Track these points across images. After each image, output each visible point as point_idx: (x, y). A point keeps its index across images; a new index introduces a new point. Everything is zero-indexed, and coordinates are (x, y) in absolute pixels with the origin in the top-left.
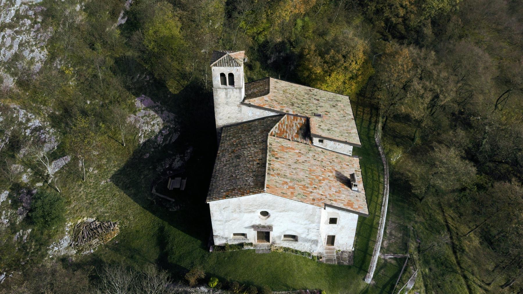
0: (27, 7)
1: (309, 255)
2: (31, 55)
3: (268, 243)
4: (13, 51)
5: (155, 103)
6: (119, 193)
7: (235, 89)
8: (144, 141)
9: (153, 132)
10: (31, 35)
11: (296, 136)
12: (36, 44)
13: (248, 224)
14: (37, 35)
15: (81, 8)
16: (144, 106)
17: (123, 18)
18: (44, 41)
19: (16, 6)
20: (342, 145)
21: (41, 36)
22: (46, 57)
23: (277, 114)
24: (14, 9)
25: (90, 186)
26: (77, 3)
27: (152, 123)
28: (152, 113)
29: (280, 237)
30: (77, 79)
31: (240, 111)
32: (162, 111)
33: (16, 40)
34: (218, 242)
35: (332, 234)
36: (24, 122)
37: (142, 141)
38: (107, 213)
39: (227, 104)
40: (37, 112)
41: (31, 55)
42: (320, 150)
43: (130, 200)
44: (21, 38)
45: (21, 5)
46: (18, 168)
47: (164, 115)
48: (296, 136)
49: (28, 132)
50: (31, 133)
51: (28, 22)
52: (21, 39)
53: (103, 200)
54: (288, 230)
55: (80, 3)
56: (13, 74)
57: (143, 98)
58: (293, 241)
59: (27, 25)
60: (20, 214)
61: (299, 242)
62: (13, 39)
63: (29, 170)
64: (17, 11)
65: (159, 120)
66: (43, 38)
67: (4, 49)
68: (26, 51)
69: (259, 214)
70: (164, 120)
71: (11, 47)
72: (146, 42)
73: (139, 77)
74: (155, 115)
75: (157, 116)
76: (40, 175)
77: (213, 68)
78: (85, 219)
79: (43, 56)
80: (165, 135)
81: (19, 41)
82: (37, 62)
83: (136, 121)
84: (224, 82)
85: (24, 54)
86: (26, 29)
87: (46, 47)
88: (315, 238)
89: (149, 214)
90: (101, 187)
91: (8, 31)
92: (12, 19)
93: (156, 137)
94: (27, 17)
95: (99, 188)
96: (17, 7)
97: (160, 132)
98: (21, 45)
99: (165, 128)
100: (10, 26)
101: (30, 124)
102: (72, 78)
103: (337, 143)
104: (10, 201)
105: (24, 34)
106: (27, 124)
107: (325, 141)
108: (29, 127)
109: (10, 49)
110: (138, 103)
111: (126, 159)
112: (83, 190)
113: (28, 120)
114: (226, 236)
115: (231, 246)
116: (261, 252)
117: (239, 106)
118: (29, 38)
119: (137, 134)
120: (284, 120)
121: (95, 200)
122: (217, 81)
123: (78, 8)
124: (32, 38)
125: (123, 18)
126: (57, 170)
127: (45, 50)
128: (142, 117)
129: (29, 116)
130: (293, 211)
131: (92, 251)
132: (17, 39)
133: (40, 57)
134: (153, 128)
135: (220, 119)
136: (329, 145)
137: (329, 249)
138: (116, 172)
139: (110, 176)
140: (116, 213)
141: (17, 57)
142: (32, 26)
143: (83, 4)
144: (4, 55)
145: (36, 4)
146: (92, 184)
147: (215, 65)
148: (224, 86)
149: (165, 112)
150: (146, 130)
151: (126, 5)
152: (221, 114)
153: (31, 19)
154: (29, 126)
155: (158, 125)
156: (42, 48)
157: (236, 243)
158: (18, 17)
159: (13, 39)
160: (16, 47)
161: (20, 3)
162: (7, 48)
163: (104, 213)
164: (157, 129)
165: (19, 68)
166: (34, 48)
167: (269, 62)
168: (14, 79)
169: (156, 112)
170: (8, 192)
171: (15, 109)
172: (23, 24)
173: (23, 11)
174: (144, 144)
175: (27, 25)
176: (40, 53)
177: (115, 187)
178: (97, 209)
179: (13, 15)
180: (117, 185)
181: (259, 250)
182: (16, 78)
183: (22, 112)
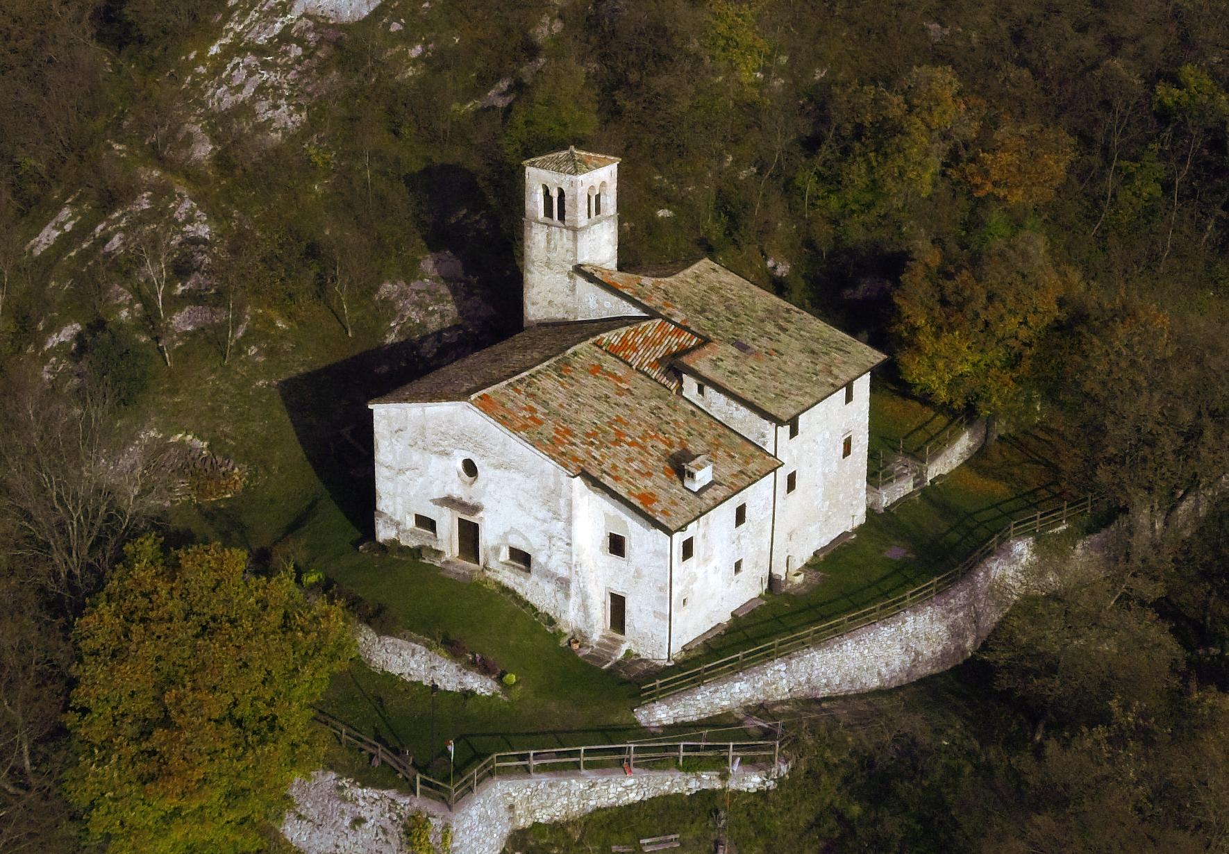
0: (311, 23)
1: (551, 622)
2: (270, 113)
3: (472, 566)
4: (241, 97)
5: (466, 274)
6: (281, 414)
7: (564, 230)
8: (397, 341)
9: (423, 325)
10: (289, 77)
11: (650, 365)
12: (287, 98)
13: (437, 493)
14: (300, 80)
15: (423, 53)
16: (436, 274)
17: (503, 94)
18: (310, 95)
19: (289, 16)
20: (744, 412)
21: (307, 84)
22: (298, 128)
23: (644, 315)
24: (283, 22)
25: (233, 379)
26: (417, 41)
27: (430, 308)
28: (444, 290)
29: (497, 550)
30: (334, 184)
31: (573, 289)
32: (470, 294)
33: (254, 78)
34: (384, 533)
35: (618, 591)
36: (180, 220)
37: (391, 338)
38: (232, 438)
39: (548, 264)
40: (215, 215)
41: (270, 113)
42: (691, 408)
43: (291, 435)
44: (266, 76)
45: (299, 18)
46: (122, 293)
47: (468, 304)
48: (650, 365)
49: (178, 238)
50: (181, 244)
51: (296, 51)
52: (264, 78)
53: (242, 414)
54: (513, 530)
55: (426, 44)
56: (215, 139)
57: (445, 258)
58: (522, 569)
59: (292, 56)
60: (78, 375)
61: (534, 577)
62: (251, 74)
63: (137, 306)
64: (288, 27)
65: (450, 308)
66: (309, 89)
67: (225, 88)
68: (263, 103)
69: (460, 466)
70: (461, 313)
71: (240, 88)
72: (504, 141)
73: (465, 216)
74: (447, 295)
75: (450, 298)
76: (153, 323)
77: (529, 170)
78: (189, 437)
79: (293, 122)
80: (445, 343)
81: (259, 81)
82: (276, 130)
83: (403, 295)
84: (548, 212)
85: (257, 107)
86: (285, 64)
87: (309, 108)
88: (563, 572)
89: (310, 472)
90: (253, 390)
91: (250, 59)
92: (270, 41)
93: (424, 338)
94: (300, 41)
95: (248, 391)
96: (292, 19)
97: (439, 334)
98: (261, 89)
99: (456, 327)
100: (259, 51)
101: (189, 228)
102: (326, 177)
103: (734, 404)
104: (74, 346)
105: (277, 72)
106: (185, 226)
107: (707, 389)
108: (183, 233)
109: (237, 92)
110: (428, 264)
111: (332, 360)
112: (213, 381)
113: (190, 220)
114: (397, 518)
115: (404, 550)
116: (452, 576)
117: (571, 277)
118: (282, 80)
119: (390, 320)
120: (645, 328)
121: (226, 407)
122: (535, 203)
123: (416, 51)
124: (288, 84)
125: (503, 94)
126: (190, 328)
127: (304, 114)
128: (418, 293)
129: (196, 215)
130: (520, 472)
131: (167, 504)
132: (258, 76)
133: (286, 123)
134: (428, 319)
135: (533, 304)
136: (717, 404)
137: (613, 639)
138: (299, 374)
139: (283, 377)
140: (250, 448)
141: (244, 110)
142: (298, 61)
143: (431, 46)
144: (220, 100)
145: (333, 25)
146: (238, 377)
147: (532, 164)
148: (548, 220)
149: (477, 298)
150: (410, 319)
151: (524, 69)
152: (535, 290)
153: (305, 49)
154: (184, 229)
155: (442, 316)
156: (299, 108)
157: (413, 543)
158: (285, 37)
159: (251, 74)
160: (248, 92)
161: (300, 14)
162: (231, 88)
163: (226, 436)
164: (434, 324)
165: (234, 131)
166: (283, 101)
167: (848, 293)
168: (214, 149)
169: (454, 292)
170: (79, 328)
171: (180, 195)
172: (286, 53)
173: (300, 30)
174: (393, 346)
175: (292, 56)
176: (290, 116)
177: (278, 400)
178: (218, 425)
179: (277, 32)
180: (285, 398)
181: (450, 572)
182: (219, 148)
183: (187, 204)
